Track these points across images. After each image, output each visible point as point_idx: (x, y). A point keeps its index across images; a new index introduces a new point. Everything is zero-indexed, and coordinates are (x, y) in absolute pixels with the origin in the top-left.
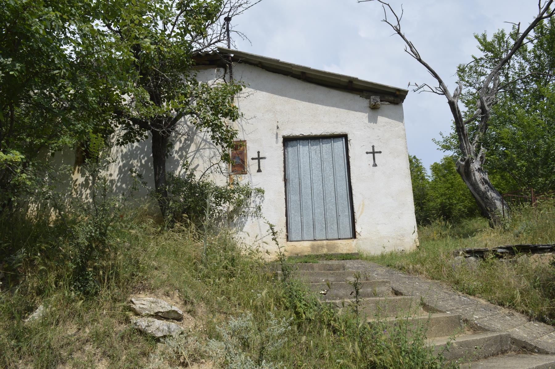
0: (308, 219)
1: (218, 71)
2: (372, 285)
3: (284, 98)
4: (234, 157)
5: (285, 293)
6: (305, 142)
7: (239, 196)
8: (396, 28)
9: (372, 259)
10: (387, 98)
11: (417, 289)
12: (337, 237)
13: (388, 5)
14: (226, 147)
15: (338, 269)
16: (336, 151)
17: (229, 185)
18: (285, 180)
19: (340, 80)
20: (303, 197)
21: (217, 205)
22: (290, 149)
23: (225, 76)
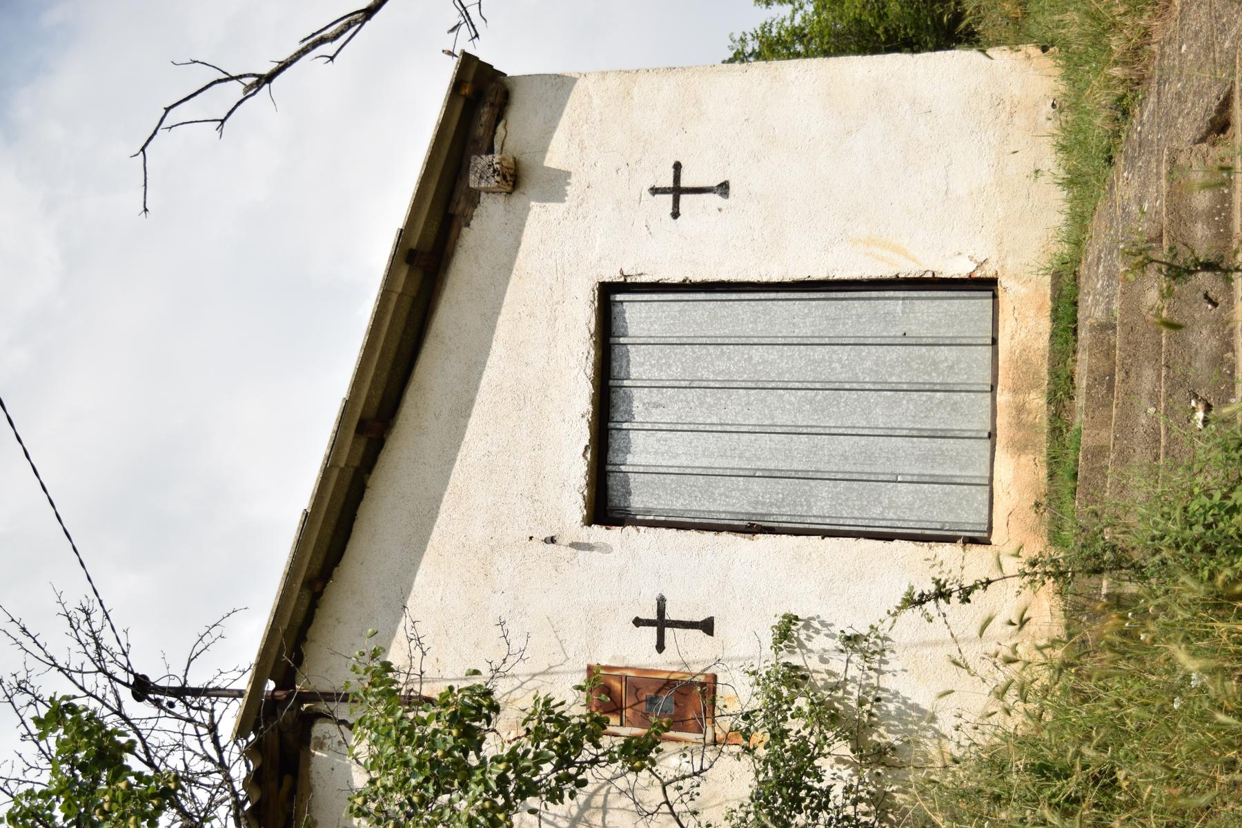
0: (908, 457)
1: (321, 746)
2: (1179, 211)
3: (443, 507)
4: (643, 720)
5: (1194, 570)
6: (616, 441)
7: (799, 713)
8: (251, 86)
9: (1080, 220)
10: (481, 131)
11: (1209, 48)
12: (988, 352)
13: (167, 110)
14: (598, 746)
15: (1108, 353)
16: (657, 330)
17: (749, 751)
18: (752, 529)
19: (401, 295)
20: (821, 467)
21: (826, 807)
22: (637, 502)
23: (344, 722)
